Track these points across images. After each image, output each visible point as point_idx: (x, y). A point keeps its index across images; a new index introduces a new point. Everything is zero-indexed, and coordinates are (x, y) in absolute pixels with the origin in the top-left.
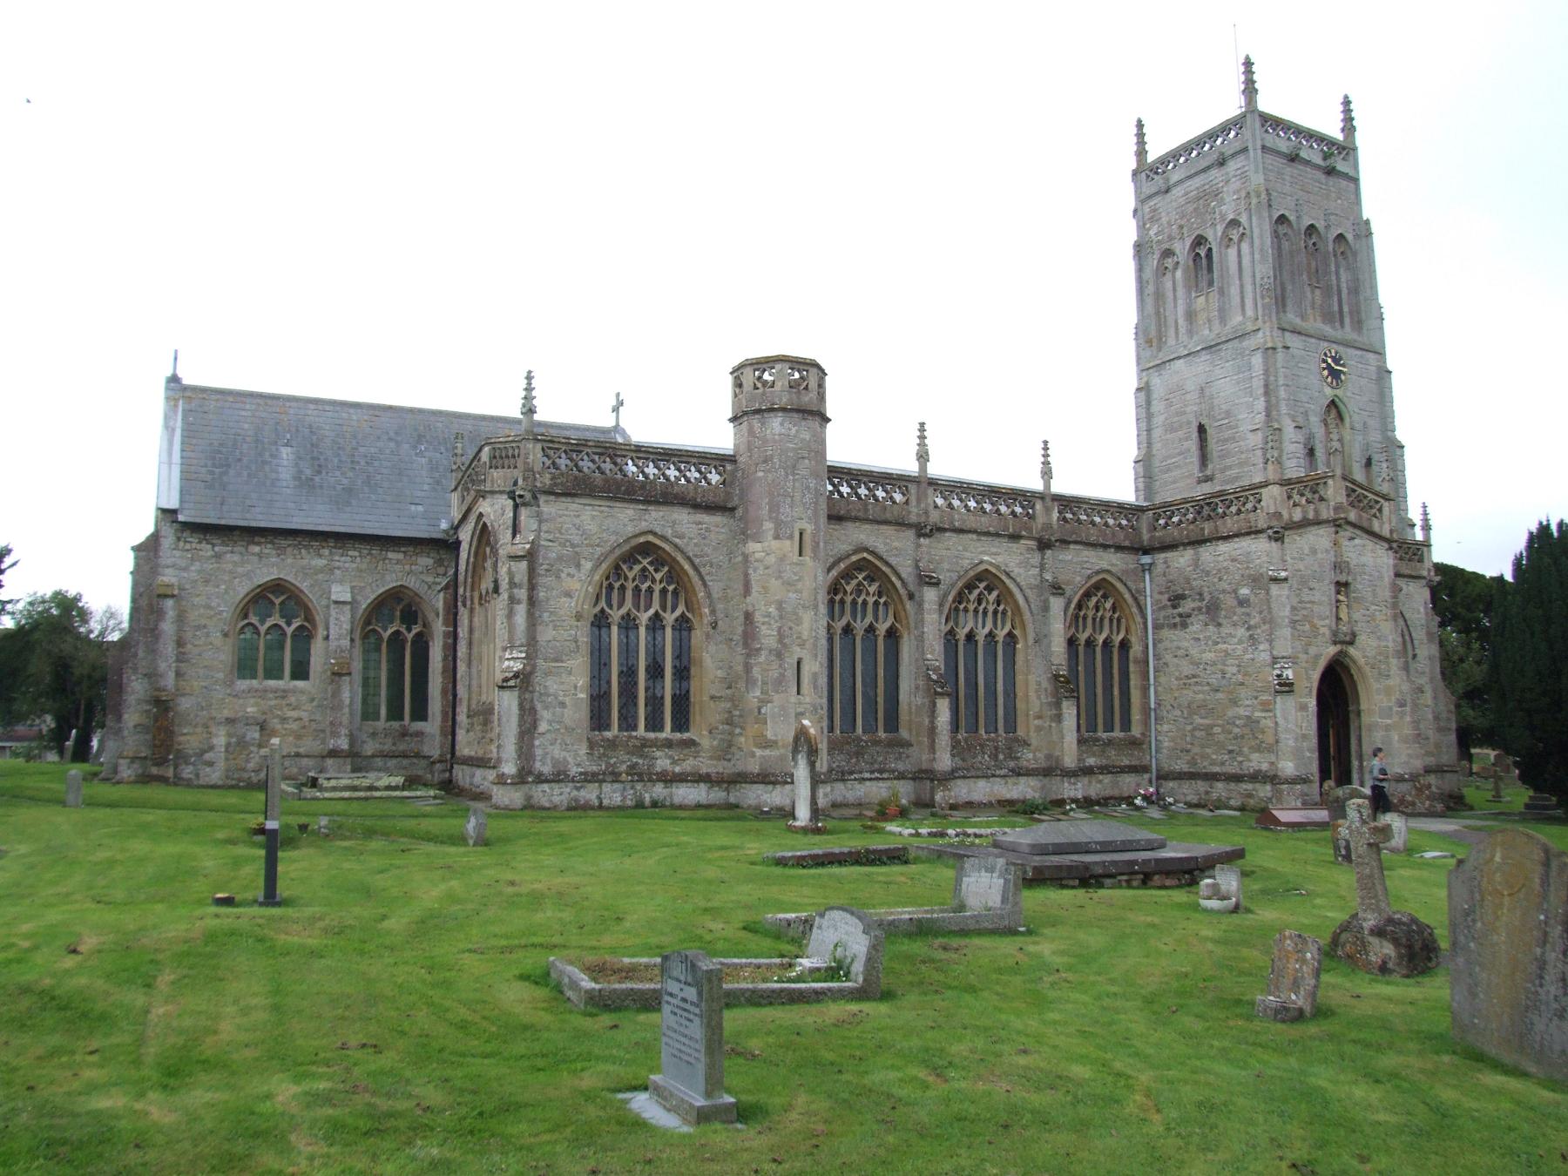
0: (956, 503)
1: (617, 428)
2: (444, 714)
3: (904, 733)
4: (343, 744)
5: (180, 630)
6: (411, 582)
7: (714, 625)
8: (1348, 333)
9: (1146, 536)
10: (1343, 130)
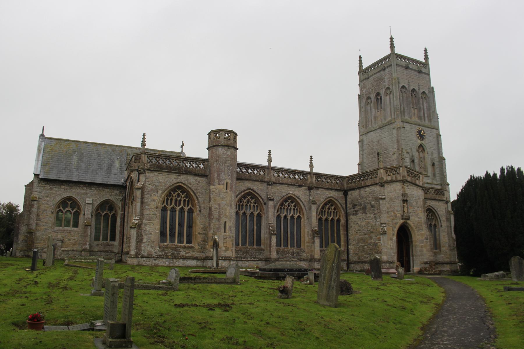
0: (281, 175)
1: (182, 152)
2: (120, 239)
3: (262, 247)
4: (87, 247)
5: (38, 211)
6: (112, 198)
7: (200, 211)
8: (427, 123)
9: (345, 186)
10: (424, 59)
